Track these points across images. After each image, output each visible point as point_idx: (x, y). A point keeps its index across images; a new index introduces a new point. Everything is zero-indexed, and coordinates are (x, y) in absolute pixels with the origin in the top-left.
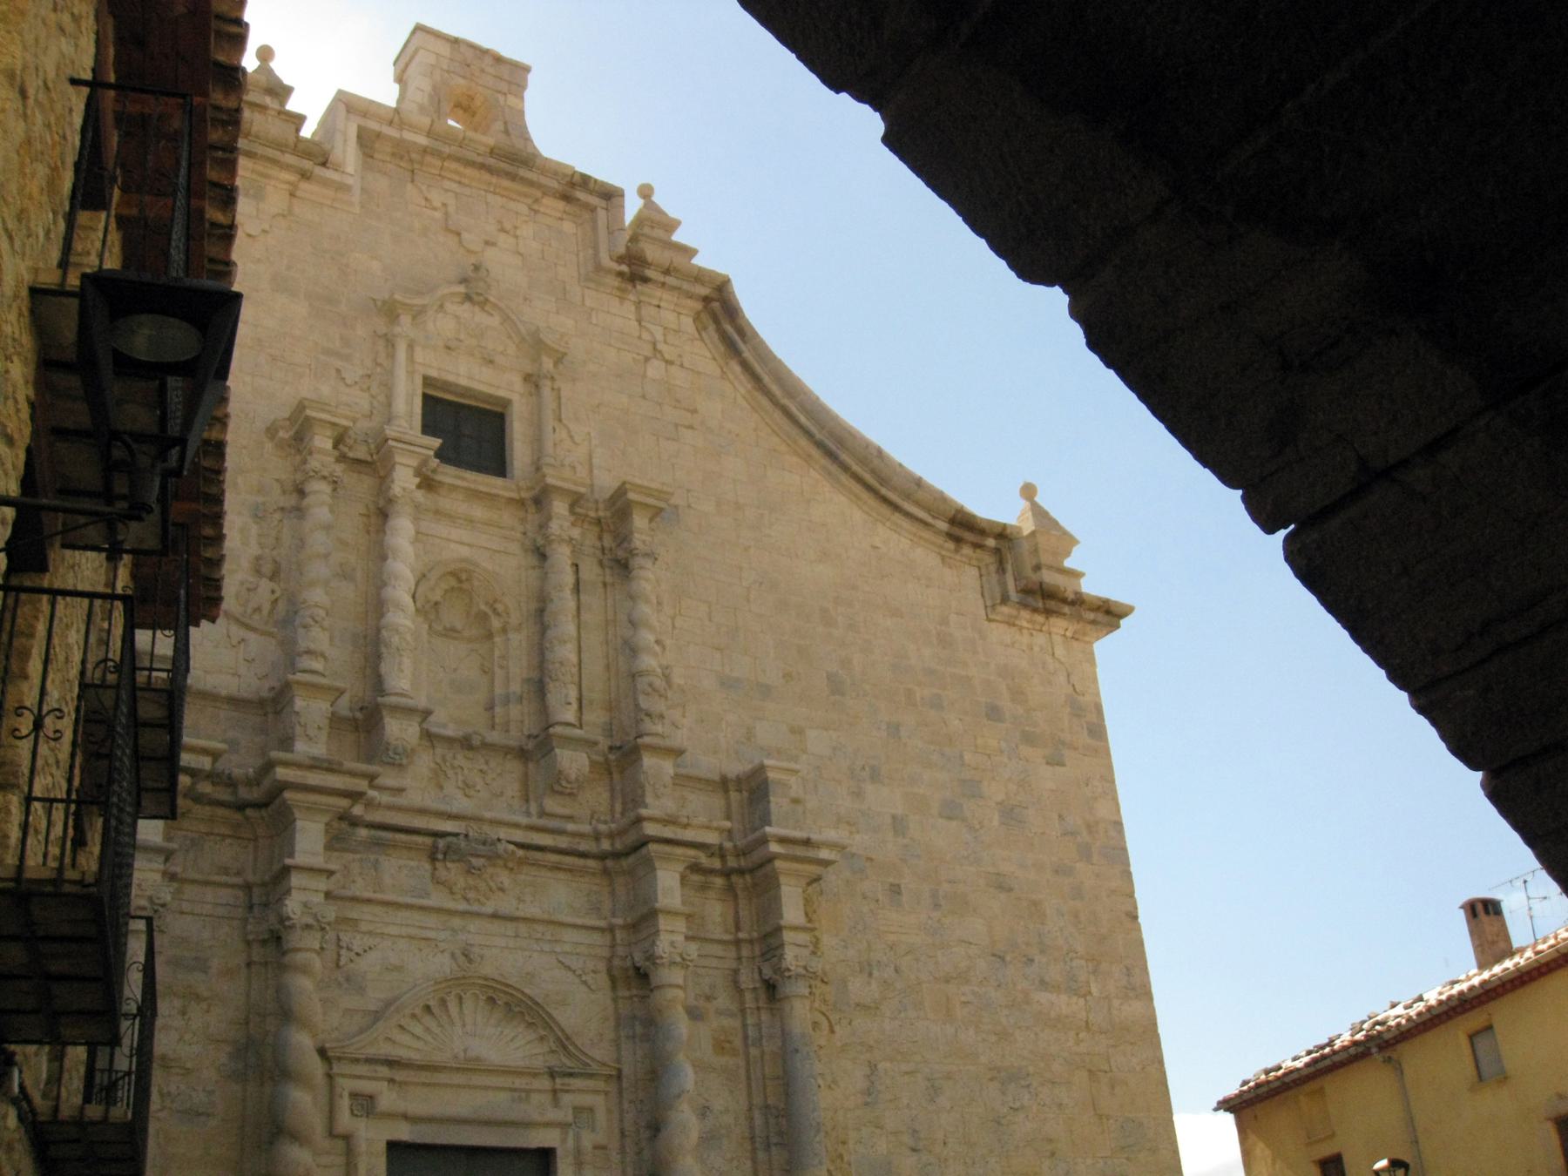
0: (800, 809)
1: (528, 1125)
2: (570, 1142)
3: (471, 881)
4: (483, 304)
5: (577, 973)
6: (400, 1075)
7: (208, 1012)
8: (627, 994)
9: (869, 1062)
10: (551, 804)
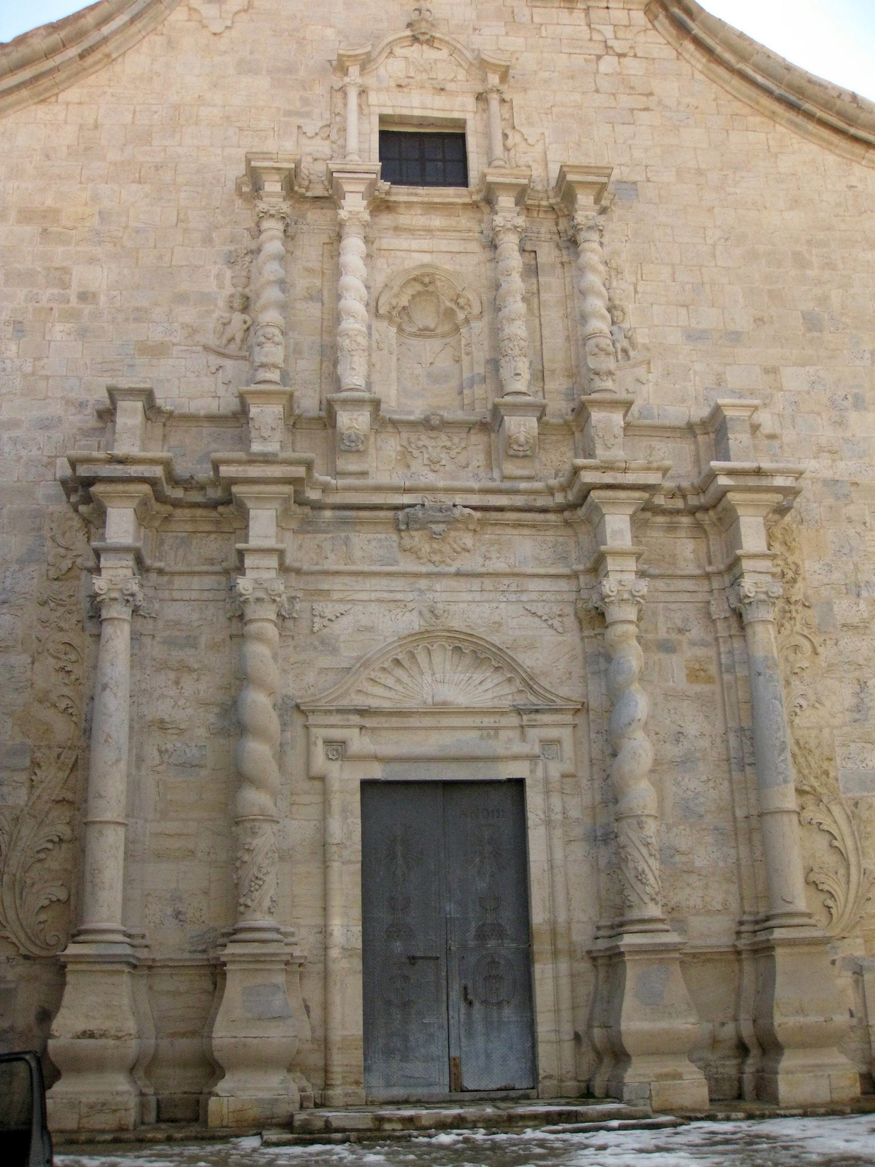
0: (776, 443)
1: (495, 759)
2: (540, 773)
3: (435, 546)
4: (430, 42)
5: (543, 618)
6: (368, 722)
7: (198, 680)
8: (592, 633)
9: (859, 680)
10: (510, 468)
